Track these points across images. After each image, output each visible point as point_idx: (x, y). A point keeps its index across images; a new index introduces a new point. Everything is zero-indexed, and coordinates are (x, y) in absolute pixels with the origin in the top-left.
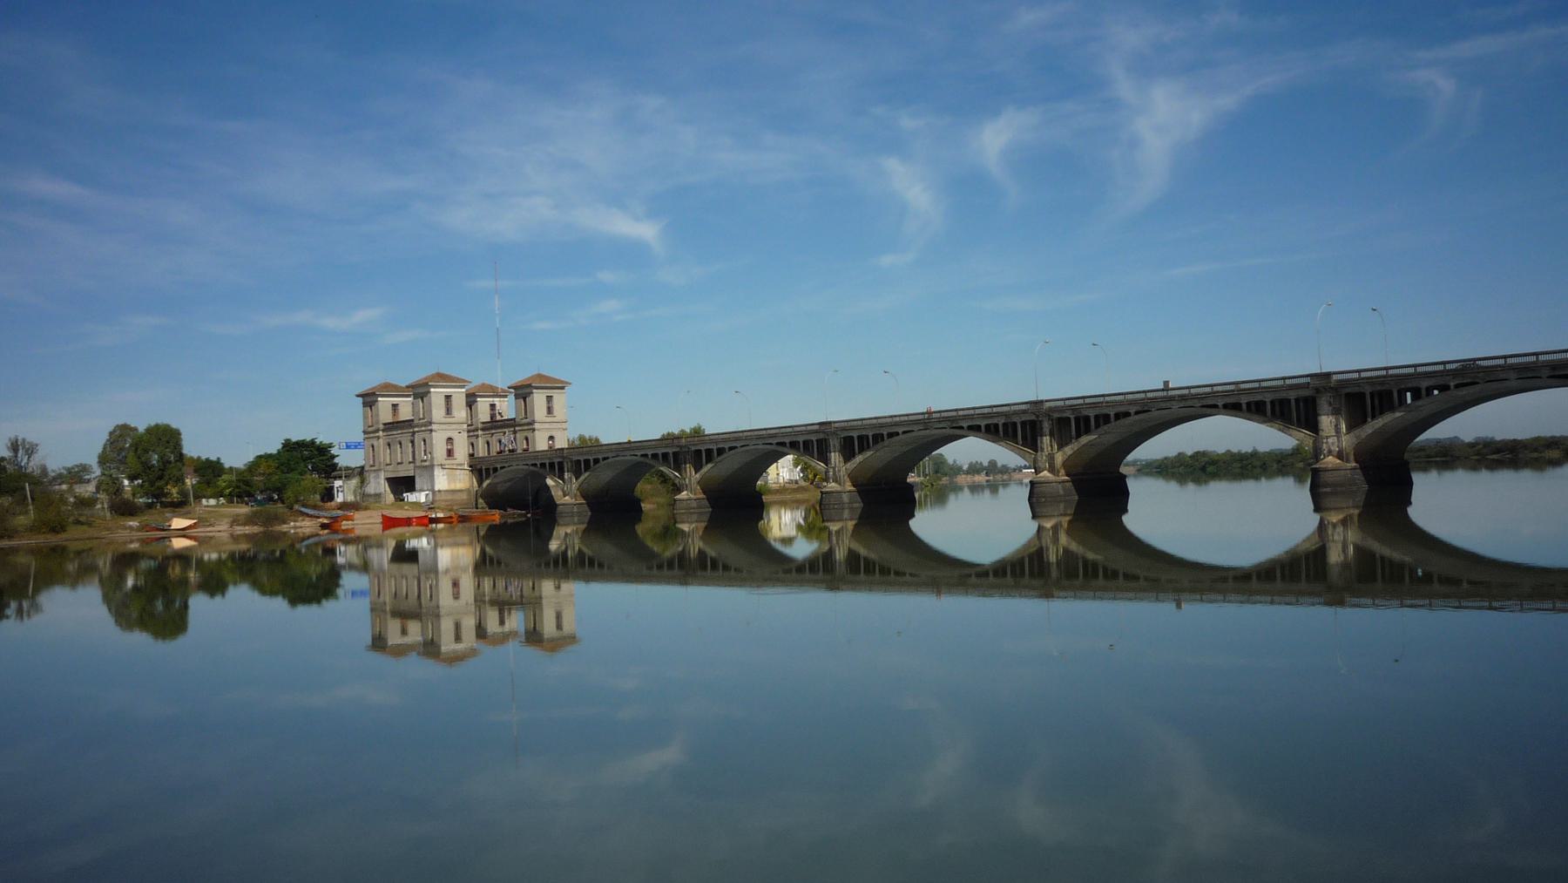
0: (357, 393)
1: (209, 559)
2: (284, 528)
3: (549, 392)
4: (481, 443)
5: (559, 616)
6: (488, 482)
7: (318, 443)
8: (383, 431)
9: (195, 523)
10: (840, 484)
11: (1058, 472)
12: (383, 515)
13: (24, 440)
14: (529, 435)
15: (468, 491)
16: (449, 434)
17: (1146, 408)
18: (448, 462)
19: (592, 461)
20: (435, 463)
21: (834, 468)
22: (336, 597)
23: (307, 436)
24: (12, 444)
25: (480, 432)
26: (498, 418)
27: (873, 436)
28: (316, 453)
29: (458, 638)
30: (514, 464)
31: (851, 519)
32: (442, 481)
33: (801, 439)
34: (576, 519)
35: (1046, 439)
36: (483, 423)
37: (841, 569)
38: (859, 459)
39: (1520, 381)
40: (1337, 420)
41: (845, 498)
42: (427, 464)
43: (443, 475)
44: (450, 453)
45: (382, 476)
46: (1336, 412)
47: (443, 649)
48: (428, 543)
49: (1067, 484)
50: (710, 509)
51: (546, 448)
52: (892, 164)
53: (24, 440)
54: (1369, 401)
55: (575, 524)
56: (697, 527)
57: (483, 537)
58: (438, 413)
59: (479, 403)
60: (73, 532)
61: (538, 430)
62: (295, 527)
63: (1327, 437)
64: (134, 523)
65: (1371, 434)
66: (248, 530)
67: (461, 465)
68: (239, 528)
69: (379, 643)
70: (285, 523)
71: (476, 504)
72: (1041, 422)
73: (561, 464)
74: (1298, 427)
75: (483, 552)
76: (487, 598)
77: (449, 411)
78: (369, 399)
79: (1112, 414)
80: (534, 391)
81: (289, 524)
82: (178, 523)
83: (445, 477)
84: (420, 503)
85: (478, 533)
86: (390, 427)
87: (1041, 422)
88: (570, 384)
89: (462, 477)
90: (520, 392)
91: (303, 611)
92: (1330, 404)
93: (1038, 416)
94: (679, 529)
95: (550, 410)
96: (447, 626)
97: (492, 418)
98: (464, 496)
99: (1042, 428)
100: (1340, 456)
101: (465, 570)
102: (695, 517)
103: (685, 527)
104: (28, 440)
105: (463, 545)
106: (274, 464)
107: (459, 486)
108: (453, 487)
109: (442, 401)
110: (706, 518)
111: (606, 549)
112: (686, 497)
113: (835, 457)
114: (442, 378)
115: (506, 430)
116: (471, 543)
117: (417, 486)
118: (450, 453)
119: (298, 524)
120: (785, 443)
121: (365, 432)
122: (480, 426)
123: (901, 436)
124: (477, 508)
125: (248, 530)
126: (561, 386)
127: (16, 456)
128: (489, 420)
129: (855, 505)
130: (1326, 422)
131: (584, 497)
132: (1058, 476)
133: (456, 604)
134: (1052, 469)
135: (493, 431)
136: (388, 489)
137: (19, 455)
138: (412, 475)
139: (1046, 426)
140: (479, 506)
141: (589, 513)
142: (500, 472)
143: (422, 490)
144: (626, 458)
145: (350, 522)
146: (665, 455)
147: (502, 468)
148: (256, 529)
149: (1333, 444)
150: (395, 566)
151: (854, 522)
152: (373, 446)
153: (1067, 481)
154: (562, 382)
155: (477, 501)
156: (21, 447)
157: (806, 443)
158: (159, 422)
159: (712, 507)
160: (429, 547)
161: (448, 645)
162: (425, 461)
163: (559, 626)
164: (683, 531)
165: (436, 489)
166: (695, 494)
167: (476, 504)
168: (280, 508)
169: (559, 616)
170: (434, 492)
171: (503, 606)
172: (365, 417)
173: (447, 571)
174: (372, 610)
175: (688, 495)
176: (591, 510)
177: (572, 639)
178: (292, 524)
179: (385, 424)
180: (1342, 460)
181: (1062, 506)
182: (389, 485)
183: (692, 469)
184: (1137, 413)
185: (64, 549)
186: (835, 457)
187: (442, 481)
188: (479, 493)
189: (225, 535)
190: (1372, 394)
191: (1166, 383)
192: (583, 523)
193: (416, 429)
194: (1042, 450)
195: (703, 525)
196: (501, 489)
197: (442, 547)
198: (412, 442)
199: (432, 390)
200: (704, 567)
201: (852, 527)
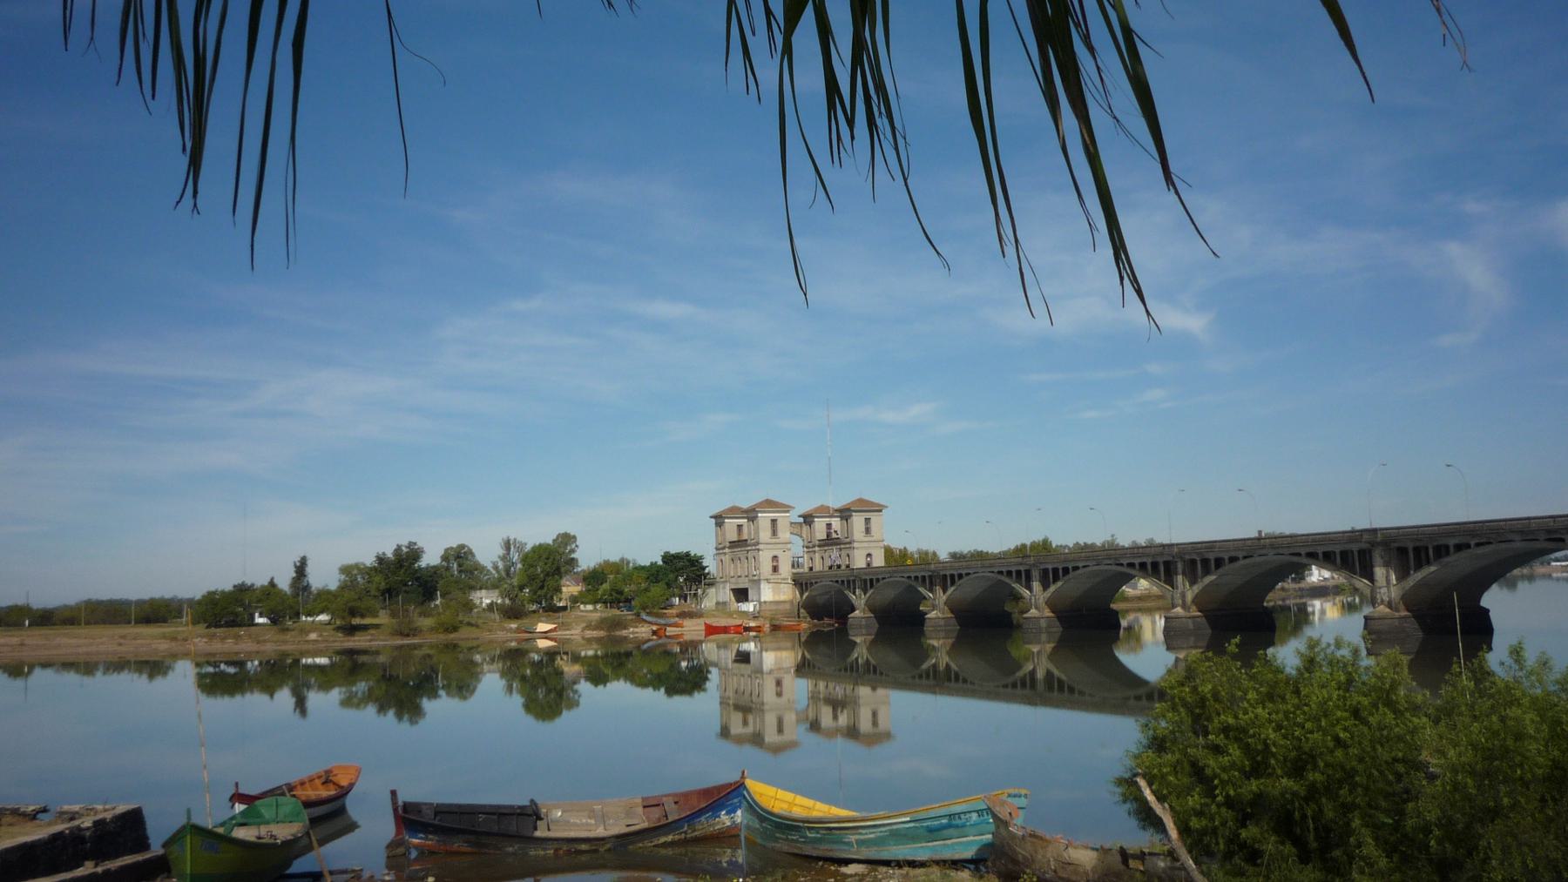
0: (711, 514)
1: (306, 662)
2: (624, 633)
3: (868, 515)
4: (817, 557)
5: (874, 714)
6: (806, 594)
7: (693, 555)
8: (729, 548)
9: (555, 628)
10: (1039, 611)
11: (1189, 608)
12: (705, 624)
13: (515, 540)
15: (791, 602)
16: (775, 553)
17: (1250, 554)
18: (774, 577)
19: (1061, 571)
20: (762, 578)
21: (1035, 596)
22: (704, 690)
24: (505, 544)
25: (817, 549)
26: (834, 536)
27: (1359, 552)
28: (688, 564)
29: (780, 730)
30: (823, 580)
31: (1049, 642)
32: (767, 593)
33: (1337, 549)
35: (1180, 578)
36: (819, 540)
37: (1040, 687)
38: (1053, 588)
39: (1524, 542)
40: (1388, 572)
41: (1043, 623)
42: (756, 578)
44: (775, 569)
45: (728, 587)
46: (1387, 565)
47: (767, 739)
48: (756, 646)
49: (1199, 620)
50: (958, 627)
51: (864, 566)
52: (1454, 249)
53: (515, 540)
54: (1411, 555)
55: (863, 635)
56: (944, 643)
57: (806, 641)
58: (765, 535)
59: (816, 523)
60: (465, 632)
61: (857, 548)
62: (633, 633)
63: (1380, 588)
64: (514, 626)
65: (1414, 586)
66: (596, 634)
67: (784, 579)
68: (588, 632)
69: (725, 732)
70: (625, 629)
72: (1176, 562)
73: (854, 581)
74: (1361, 576)
75: (803, 656)
76: (822, 696)
77: (774, 533)
78: (719, 519)
79: (1226, 558)
80: (854, 514)
81: (628, 629)
82: (543, 627)
83: (770, 590)
85: (800, 640)
86: (733, 544)
87: (1176, 562)
88: (886, 507)
89: (785, 590)
90: (844, 514)
91: (680, 701)
92: (1382, 558)
93: (1173, 557)
94: (929, 645)
95: (868, 531)
96: (770, 720)
97: (828, 536)
98: (788, 606)
99: (1176, 568)
100: (1389, 605)
101: (787, 671)
102: (942, 634)
103: (935, 643)
104: (519, 539)
106: (644, 575)
107: (782, 598)
109: (769, 524)
110: (955, 634)
111: (892, 658)
112: (934, 616)
113: (1036, 585)
114: (769, 504)
115: (834, 548)
116: (793, 648)
117: (750, 598)
118: (775, 569)
119: (636, 630)
120: (1317, 554)
121: (717, 549)
122: (817, 543)
123: (1242, 562)
125: (596, 634)
126: (878, 509)
127: (509, 554)
128: (825, 537)
129: (1054, 630)
130: (1379, 572)
132: (1189, 612)
133: (779, 700)
134: (1184, 606)
135: (826, 548)
136: (733, 598)
137: (511, 552)
139: (1180, 566)
140: (801, 615)
141: (877, 625)
142: (1072, 574)
143: (752, 601)
144: (896, 579)
145: (680, 629)
146: (1019, 573)
147: (816, 583)
148: (602, 633)
149: (1384, 594)
150: (736, 665)
151: (1052, 645)
152: (722, 561)
153: (1198, 617)
154: (879, 505)
155: (799, 610)
156: (512, 547)
157: (1344, 554)
158: (542, 542)
159: (960, 625)
160: (756, 650)
161: (771, 736)
162: (755, 576)
163: (875, 723)
164: (933, 646)
165: (762, 600)
166: (943, 613)
168: (626, 614)
169: (874, 714)
170: (760, 603)
171: (836, 705)
172: (717, 535)
173: (771, 672)
174: (721, 703)
175: (937, 614)
176: (879, 623)
177: (887, 736)
178: (631, 629)
179: (730, 542)
180: (1391, 609)
181: (1192, 639)
182: (734, 595)
183: (941, 591)
184: (1245, 557)
185: (455, 646)
186: (1036, 585)
187: (767, 593)
188: (800, 604)
189: (578, 638)
190: (1359, 552)
191: (1260, 532)
192: (870, 635)
193: (749, 548)
194: (1177, 588)
195: (950, 641)
196: (821, 600)
197: (766, 650)
198: (747, 558)
199: (760, 515)
200: (949, 680)
201: (1050, 649)
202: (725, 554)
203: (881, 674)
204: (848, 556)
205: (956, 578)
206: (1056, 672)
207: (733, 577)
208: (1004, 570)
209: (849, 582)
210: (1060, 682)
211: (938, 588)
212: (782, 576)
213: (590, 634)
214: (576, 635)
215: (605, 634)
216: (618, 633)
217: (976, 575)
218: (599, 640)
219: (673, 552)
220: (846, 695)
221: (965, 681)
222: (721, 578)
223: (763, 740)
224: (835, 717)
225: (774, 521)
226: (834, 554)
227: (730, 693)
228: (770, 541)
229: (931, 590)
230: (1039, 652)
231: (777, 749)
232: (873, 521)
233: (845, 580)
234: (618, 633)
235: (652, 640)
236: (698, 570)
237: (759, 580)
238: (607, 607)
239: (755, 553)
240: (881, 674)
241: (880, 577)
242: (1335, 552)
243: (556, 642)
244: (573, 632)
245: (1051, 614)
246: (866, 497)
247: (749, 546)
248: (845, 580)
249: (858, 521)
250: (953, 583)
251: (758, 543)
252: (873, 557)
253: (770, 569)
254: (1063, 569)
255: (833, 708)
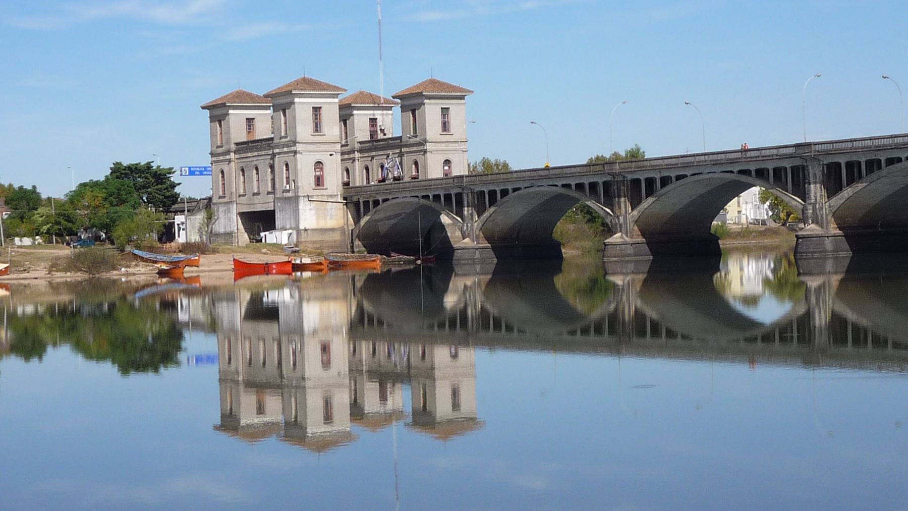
2: (114, 275)
4: (358, 168)
5: (455, 393)
12: (234, 260)
14: (419, 158)
15: (342, 230)
16: (318, 157)
21: (814, 205)
22: (177, 363)
23: (142, 160)
25: (357, 155)
26: (380, 136)
27: (867, 162)
29: (328, 418)
31: (836, 273)
34: (478, 268)
36: (361, 143)
37: (821, 339)
38: (847, 192)
41: (829, 244)
42: (290, 194)
43: (311, 209)
44: (319, 181)
45: (234, 210)
51: (441, 176)
56: (633, 280)
58: (304, 130)
59: (355, 117)
62: (127, 274)
67: (331, 196)
68: (59, 274)
70: (114, 269)
71: (352, 247)
75: (360, 309)
77: (317, 127)
80: (426, 101)
83: (313, 212)
84: (281, 244)
86: (245, 147)
95: (445, 126)
96: (314, 401)
97: (372, 136)
98: (337, 236)
103: (618, 280)
105: (335, 298)
107: (330, 223)
108: (322, 225)
110: (646, 268)
112: (620, 240)
113: (816, 191)
114: (310, 85)
115: (390, 152)
117: (278, 224)
118: (319, 181)
120: (750, 171)
121: (212, 154)
122: (357, 146)
124: (353, 252)
129: (842, 254)
131: (488, 239)
133: (325, 374)
135: (374, 153)
138: (272, 209)
140: (356, 250)
141: (495, 260)
146: (593, 186)
147: (385, 200)
148: (79, 276)
150: (251, 325)
151: (839, 277)
152: (222, 172)
154: (461, 90)
157: (777, 171)
161: (315, 426)
162: (288, 191)
163: (456, 405)
165: (302, 227)
167: (352, 247)
168: (108, 249)
169: (455, 393)
170: (298, 231)
172: (213, 135)
173: (315, 332)
174: (220, 380)
177: (471, 422)
179: (237, 144)
183: (628, 204)
186: (816, 191)
189: (42, 283)
190: (792, 168)
195: (642, 277)
196: (383, 228)
197: (308, 300)
198: (272, 167)
201: (837, 283)
202: (230, 161)
203: (509, 328)
204: (416, 163)
205: (371, 206)
206: (851, 316)
207: (258, 194)
208: (752, 168)
209: (448, 197)
210: (856, 328)
211: (623, 199)
212: (329, 192)
213: (61, 277)
214: (41, 278)
215: (86, 276)
216: (105, 275)
217: (696, 178)
218: (72, 287)
219: (125, 163)
220: (409, 366)
221: (670, 334)
222: (220, 197)
223: (303, 429)
224: (383, 398)
225: (317, 110)
226: (392, 165)
227: (240, 365)
228: (312, 139)
229: (609, 203)
230: (819, 289)
231: (323, 445)
232: (452, 113)
233: (442, 194)
234: (105, 275)
235: (155, 284)
236: (167, 188)
237: (297, 198)
238: (51, 242)
239: (289, 158)
240: (509, 328)
241: (510, 187)
242: (786, 169)
243: (7, 289)
244: (33, 274)
245: (838, 232)
246: (438, 78)
247: (277, 146)
248: (442, 194)
249: (431, 111)
250: (650, 192)
251: (295, 143)
252: (453, 165)
253: (312, 181)
254: (445, 196)
255: (380, 385)
